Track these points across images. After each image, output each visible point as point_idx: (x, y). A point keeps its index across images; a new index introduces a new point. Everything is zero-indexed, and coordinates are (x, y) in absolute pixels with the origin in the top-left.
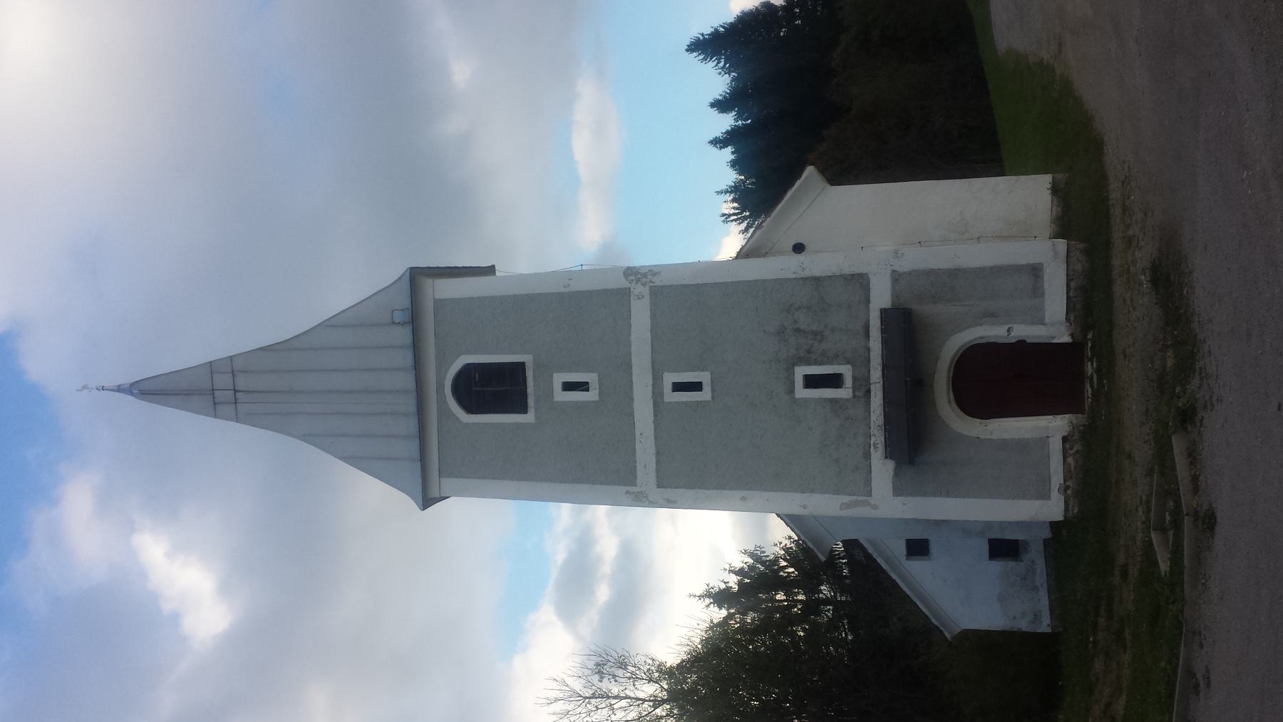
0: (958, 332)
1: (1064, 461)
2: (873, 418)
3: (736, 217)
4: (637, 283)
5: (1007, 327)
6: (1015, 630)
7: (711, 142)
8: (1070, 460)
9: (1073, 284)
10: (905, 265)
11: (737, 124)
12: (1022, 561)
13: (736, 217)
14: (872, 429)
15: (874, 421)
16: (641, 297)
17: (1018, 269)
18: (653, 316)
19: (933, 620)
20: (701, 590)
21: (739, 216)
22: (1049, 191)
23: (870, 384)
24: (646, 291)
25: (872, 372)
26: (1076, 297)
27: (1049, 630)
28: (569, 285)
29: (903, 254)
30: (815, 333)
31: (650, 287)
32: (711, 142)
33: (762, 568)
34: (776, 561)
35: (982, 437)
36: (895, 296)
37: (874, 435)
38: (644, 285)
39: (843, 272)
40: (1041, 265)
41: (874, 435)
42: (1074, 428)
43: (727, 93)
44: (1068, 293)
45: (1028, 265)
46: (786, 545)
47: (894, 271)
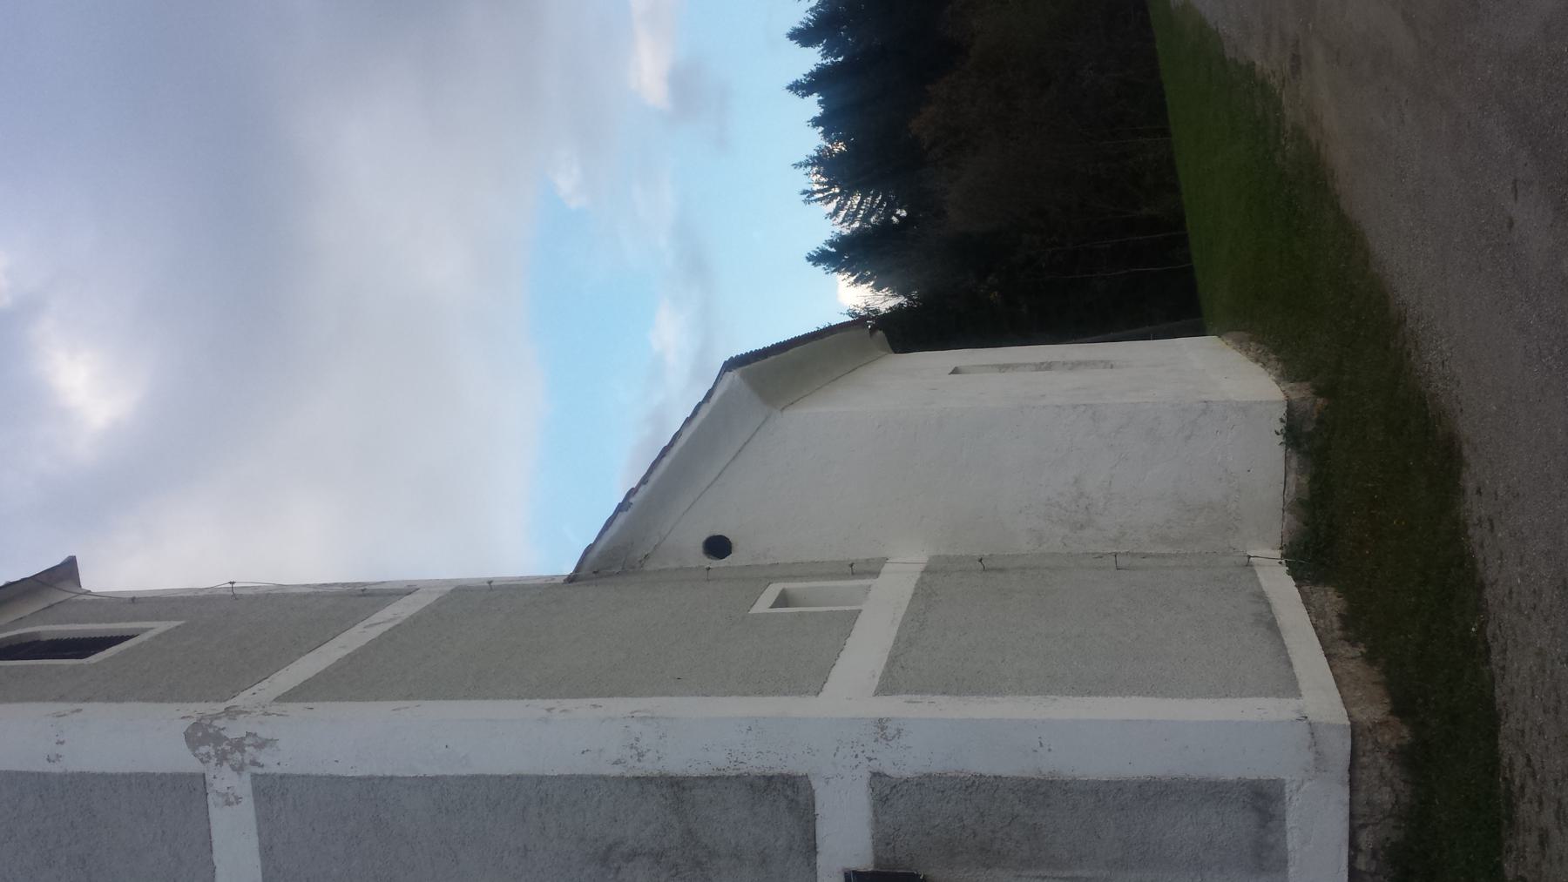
3: (821, 195)
4: (220, 763)
7: (790, 88)
9: (1365, 839)
10: (906, 761)
11: (824, 62)
13: (821, 195)
16: (232, 799)
17: (1214, 792)
18: (266, 851)
21: (826, 194)
22: (1280, 439)
24: (242, 785)
28: (58, 756)
29: (899, 731)
31: (254, 776)
32: (790, 88)
36: (883, 840)
38: (239, 769)
39: (743, 769)
40: (1279, 784)
43: (810, 20)
45: (1241, 783)
47: (876, 775)
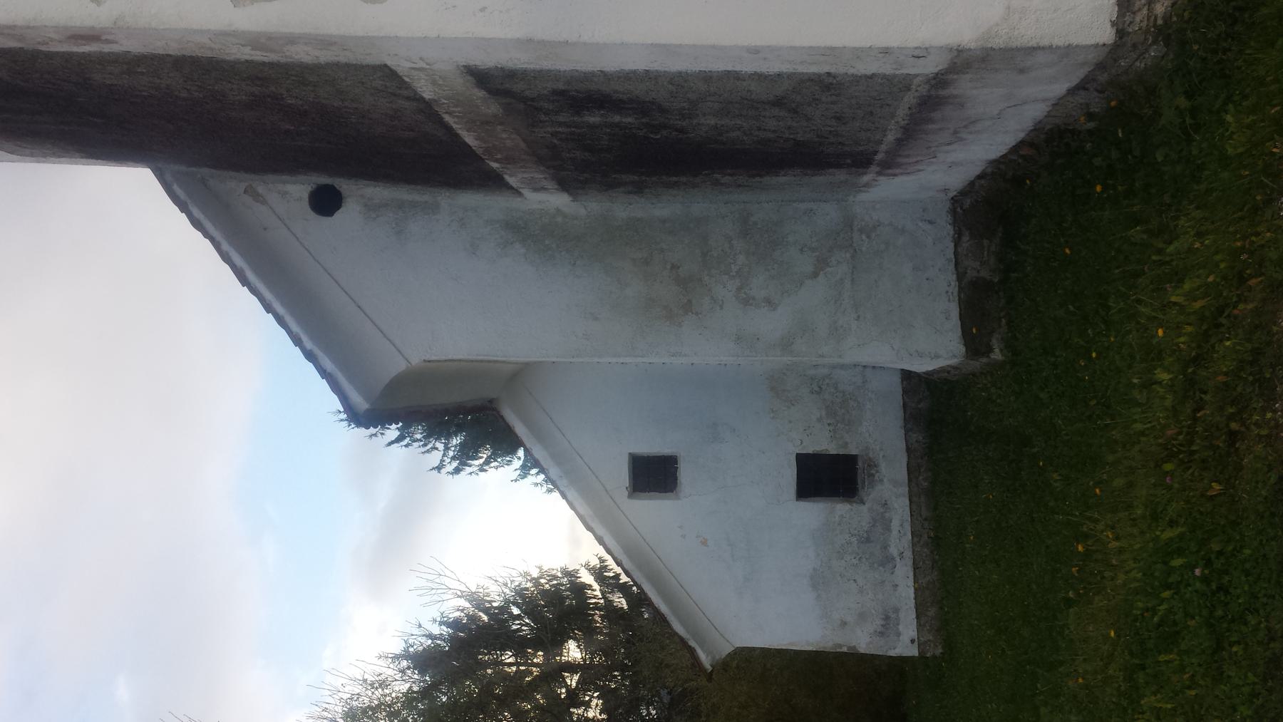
6: (845, 649)
12: (863, 502)
19: (678, 627)
20: (398, 648)
27: (913, 651)
33: (485, 618)
34: (504, 609)
46: (520, 584)
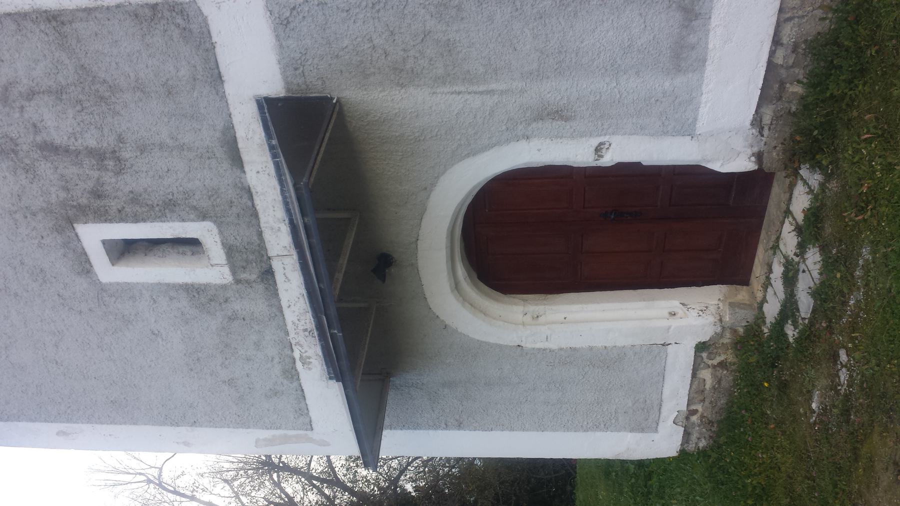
0: (468, 156)
1: (694, 375)
2: (290, 316)
5: (595, 142)
8: (706, 375)
9: (789, 34)
14: (292, 335)
15: (293, 323)
23: (269, 258)
25: (268, 236)
26: (788, 68)
30: (99, 156)
35: (528, 345)
37: (298, 344)
41: (298, 344)
42: (723, 328)
44: (772, 53)
